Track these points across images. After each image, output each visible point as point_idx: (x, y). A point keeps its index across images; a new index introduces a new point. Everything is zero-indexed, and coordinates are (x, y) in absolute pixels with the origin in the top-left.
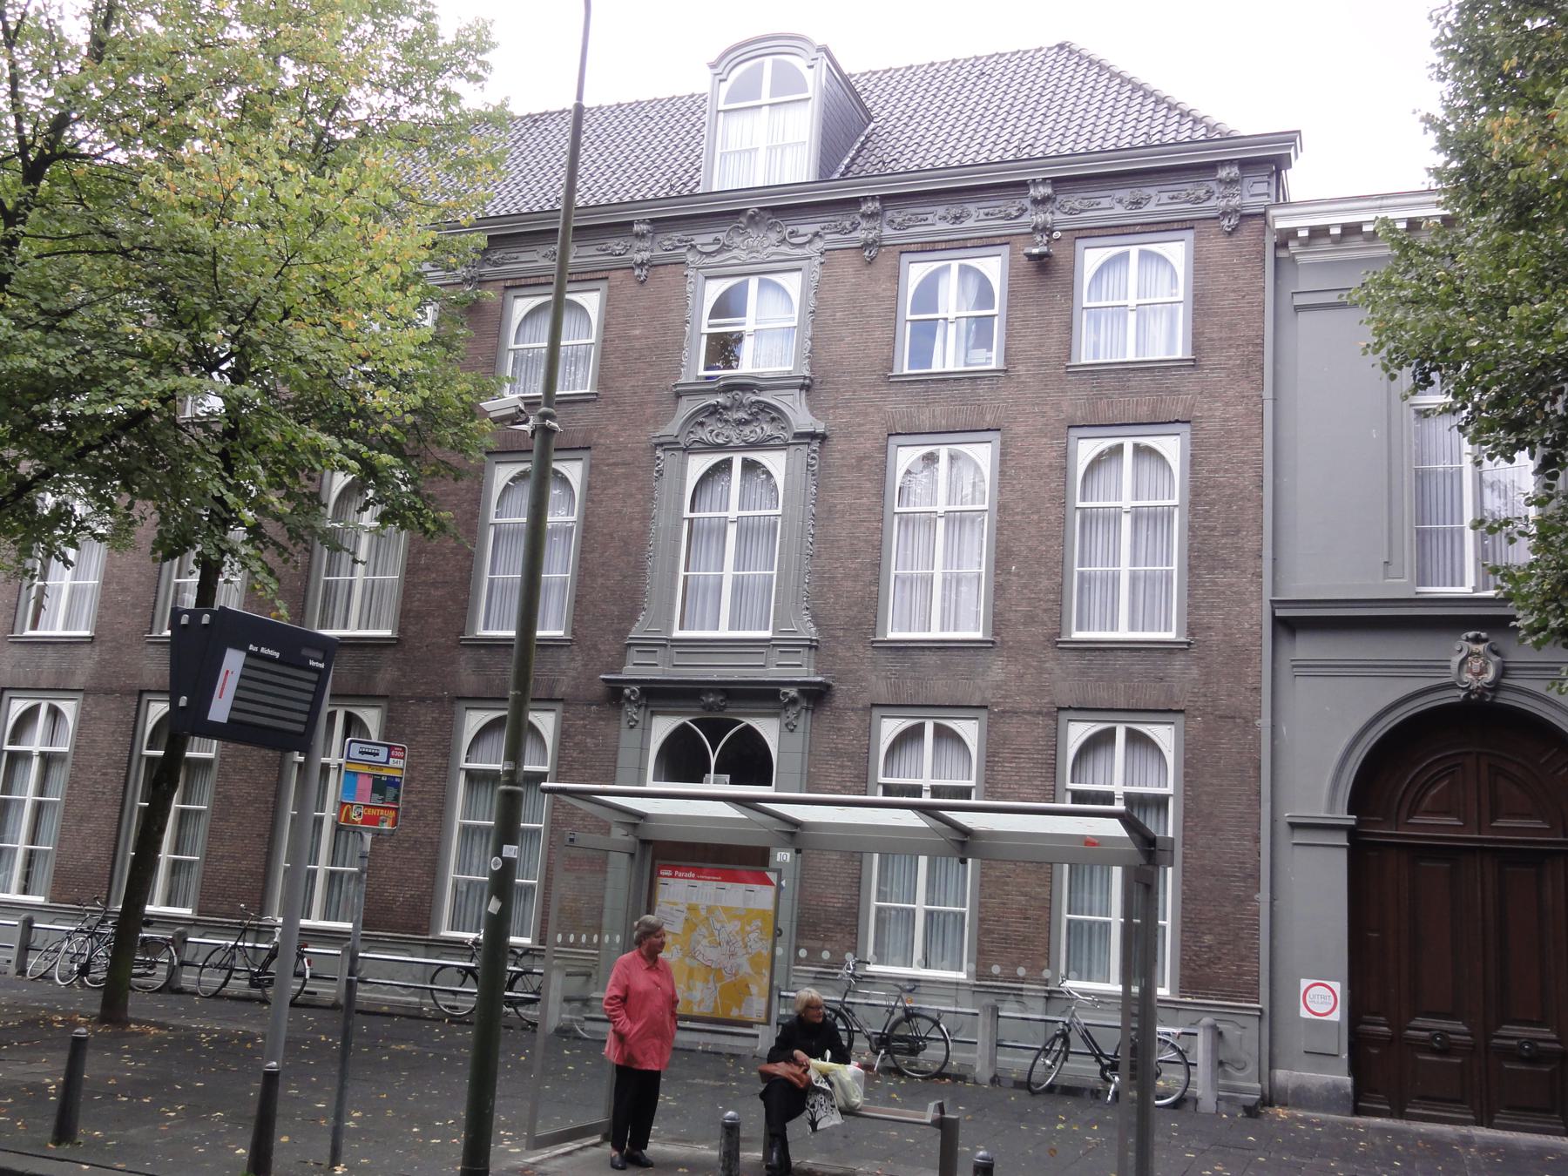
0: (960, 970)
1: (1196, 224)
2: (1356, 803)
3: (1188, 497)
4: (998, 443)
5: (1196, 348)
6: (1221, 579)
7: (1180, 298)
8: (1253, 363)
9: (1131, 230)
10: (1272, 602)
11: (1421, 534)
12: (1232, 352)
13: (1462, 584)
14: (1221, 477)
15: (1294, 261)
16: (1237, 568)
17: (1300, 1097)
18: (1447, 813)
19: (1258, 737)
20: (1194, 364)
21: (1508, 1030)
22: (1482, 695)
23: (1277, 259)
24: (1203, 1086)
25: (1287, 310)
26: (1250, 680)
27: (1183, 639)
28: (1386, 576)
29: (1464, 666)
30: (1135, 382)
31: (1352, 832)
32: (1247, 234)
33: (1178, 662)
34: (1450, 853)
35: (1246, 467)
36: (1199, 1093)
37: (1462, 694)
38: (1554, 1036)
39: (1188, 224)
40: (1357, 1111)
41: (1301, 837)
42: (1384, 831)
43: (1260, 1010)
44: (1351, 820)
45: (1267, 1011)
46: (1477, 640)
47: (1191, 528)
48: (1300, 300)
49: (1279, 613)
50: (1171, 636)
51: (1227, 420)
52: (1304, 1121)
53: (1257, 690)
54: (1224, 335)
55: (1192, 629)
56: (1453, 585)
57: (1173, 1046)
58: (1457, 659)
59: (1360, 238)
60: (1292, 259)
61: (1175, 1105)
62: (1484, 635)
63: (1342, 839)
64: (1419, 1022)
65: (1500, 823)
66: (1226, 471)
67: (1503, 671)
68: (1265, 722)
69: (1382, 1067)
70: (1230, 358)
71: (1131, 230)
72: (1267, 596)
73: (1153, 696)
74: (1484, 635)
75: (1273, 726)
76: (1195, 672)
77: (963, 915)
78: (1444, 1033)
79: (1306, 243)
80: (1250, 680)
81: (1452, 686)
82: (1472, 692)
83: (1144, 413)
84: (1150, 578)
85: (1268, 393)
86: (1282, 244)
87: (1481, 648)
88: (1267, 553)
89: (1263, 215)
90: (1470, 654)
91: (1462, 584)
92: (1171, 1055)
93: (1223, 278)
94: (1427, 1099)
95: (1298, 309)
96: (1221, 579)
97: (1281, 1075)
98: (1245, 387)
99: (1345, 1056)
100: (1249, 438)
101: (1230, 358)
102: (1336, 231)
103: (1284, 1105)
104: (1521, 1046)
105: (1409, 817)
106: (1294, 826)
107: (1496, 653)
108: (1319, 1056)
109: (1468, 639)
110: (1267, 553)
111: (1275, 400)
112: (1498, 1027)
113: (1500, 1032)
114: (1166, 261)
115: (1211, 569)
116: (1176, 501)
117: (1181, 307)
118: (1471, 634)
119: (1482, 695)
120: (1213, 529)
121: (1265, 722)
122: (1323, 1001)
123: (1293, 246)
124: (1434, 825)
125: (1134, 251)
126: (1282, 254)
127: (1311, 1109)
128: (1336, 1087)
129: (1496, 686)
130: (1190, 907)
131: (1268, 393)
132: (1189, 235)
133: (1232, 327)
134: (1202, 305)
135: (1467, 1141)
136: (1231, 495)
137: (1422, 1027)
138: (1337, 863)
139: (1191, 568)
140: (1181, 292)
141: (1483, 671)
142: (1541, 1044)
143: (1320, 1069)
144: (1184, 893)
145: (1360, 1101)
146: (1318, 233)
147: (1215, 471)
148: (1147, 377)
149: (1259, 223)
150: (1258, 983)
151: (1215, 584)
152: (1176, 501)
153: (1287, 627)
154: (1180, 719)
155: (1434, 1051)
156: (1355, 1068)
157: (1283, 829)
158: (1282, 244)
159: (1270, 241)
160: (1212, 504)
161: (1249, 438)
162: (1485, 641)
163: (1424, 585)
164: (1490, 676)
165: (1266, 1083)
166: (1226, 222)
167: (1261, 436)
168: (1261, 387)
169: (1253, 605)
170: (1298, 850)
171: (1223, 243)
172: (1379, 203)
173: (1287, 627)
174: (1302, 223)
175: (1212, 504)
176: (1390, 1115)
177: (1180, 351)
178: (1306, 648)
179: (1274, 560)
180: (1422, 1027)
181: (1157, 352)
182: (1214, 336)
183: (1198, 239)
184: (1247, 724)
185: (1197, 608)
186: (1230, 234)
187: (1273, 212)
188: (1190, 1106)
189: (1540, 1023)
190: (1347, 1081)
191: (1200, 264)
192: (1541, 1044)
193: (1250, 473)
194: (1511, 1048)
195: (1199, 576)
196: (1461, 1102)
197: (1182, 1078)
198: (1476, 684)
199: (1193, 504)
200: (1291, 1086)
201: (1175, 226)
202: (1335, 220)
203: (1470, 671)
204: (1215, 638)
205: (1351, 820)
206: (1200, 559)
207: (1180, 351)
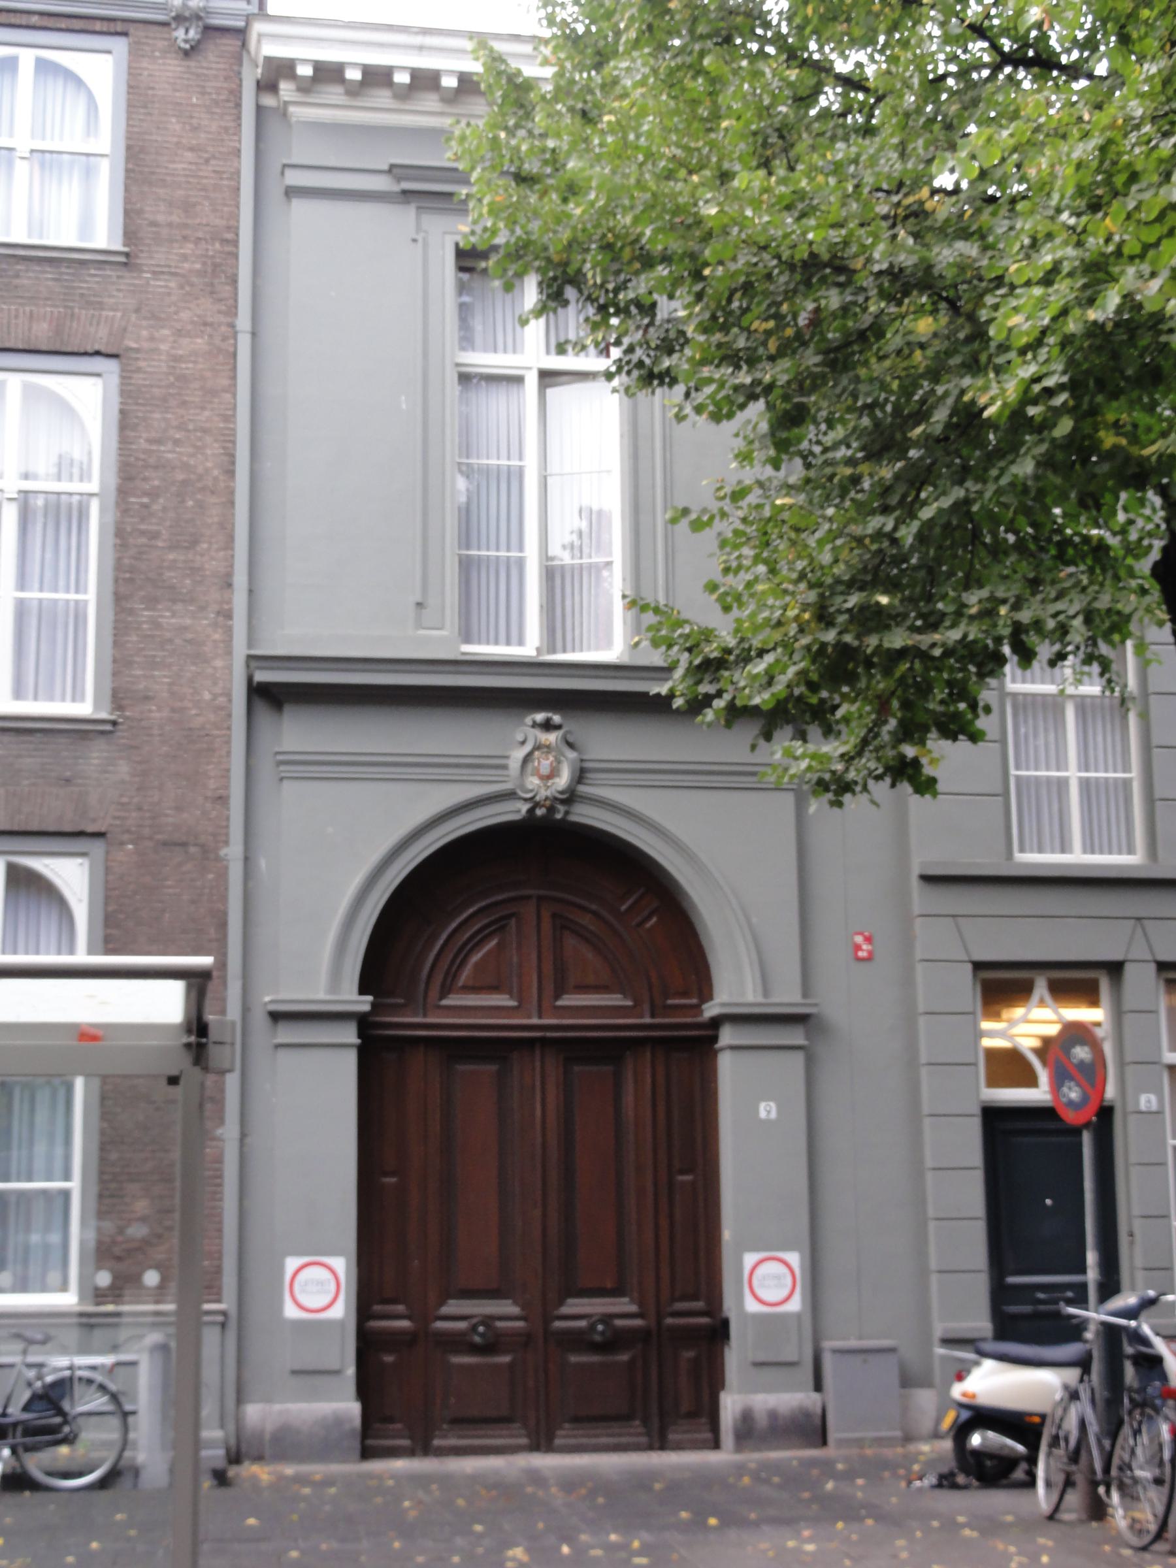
0: (64, 1288)
1: (132, 29)
2: (372, 977)
3: (113, 481)
4: (115, 380)
5: (129, 235)
6: (168, 619)
7: (106, 148)
8: (219, 273)
9: (24, 20)
10: (250, 658)
11: (467, 566)
12: (189, 248)
13: (521, 643)
14: (168, 453)
15: (285, 114)
16: (192, 601)
17: (284, 1444)
18: (495, 988)
19: (223, 875)
20: (127, 261)
21: (575, 1305)
22: (551, 810)
23: (259, 109)
24: (149, 1449)
25: (274, 192)
26: (212, 784)
27: (104, 715)
28: (419, 625)
29: (526, 767)
30: (28, 278)
31: (364, 1023)
32: (214, 57)
33: (97, 753)
34: (495, 1049)
35: (208, 439)
36: (141, 1457)
37: (524, 808)
38: (633, 1308)
39: (119, 27)
40: (367, 1453)
41: (288, 1033)
42: (409, 1020)
43: (224, 1313)
44: (364, 1004)
45: (233, 1313)
46: (547, 726)
47: (120, 533)
48: (294, 178)
49: (261, 677)
50: (84, 709)
51: (177, 359)
52: (300, 1480)
53: (222, 800)
54: (175, 219)
55: (118, 698)
56: (508, 643)
57: (102, 1388)
58: (519, 754)
59: (339, 89)
60: (282, 112)
61: (103, 1484)
62: (557, 719)
63: (349, 1034)
64: (453, 1307)
65: (567, 1001)
66: (177, 442)
67: (581, 775)
68: (233, 851)
69: (404, 1385)
70: (185, 258)
71: (24, 20)
72: (240, 651)
73: (54, 810)
74: (557, 719)
75: (246, 859)
76: (123, 769)
77: (66, 1195)
78: (488, 1320)
79: (307, 87)
80: (212, 784)
81: (510, 795)
82: (537, 805)
83: (41, 333)
84: (48, 614)
85: (243, 322)
86: (267, 86)
87: (552, 737)
88: (240, 579)
89: (241, 33)
90: (538, 747)
91: (521, 643)
92: (99, 1402)
93: (174, 125)
94: (461, 1422)
95: (291, 192)
96: (168, 619)
97: (253, 1412)
98: (206, 307)
99: (351, 1371)
100: (214, 393)
101: (185, 258)
102: (449, 82)
103: (259, 1458)
104: (592, 1327)
105: (442, 997)
106: (276, 1017)
107: (571, 745)
108: (310, 1375)
109: (535, 725)
110: (240, 579)
111: (254, 334)
112: (561, 1303)
113: (565, 1310)
114: (79, 82)
115: (152, 602)
116: (93, 486)
117: (104, 166)
118: (540, 717)
119: (551, 810)
120: (155, 536)
121: (233, 851)
122: (319, 1288)
123: (286, 89)
124: (474, 1006)
125: (27, 58)
126: (268, 101)
127: (301, 1460)
128: (339, 1420)
129: (570, 797)
130: (114, 1156)
131: (243, 322)
132: (120, 45)
133: (188, 207)
134: (140, 165)
135: (536, 1478)
136: (184, 483)
137: (460, 1313)
138: (344, 1069)
139: (118, 598)
140: (105, 139)
141: (554, 773)
142: (499, 1324)
143: (313, 1395)
144: (102, 1133)
145: (371, 1440)
146: (328, 73)
147: (158, 442)
148: (49, 273)
149: (230, 44)
150: (218, 1271)
151: (157, 625)
152: (93, 486)
153: (268, 696)
154: (97, 848)
155: (475, 1349)
156: (364, 1390)
157: (260, 1020)
158: (267, 86)
159: (250, 75)
160: (154, 494)
161: (214, 393)
162: (558, 727)
163: (468, 640)
164: (563, 781)
165: (231, 1427)
166: (180, 34)
167: (232, 389)
168: (233, 311)
169: (219, 663)
170: (282, 1054)
171: (174, 66)
172: (419, 40)
173: (268, 696)
174: (305, 54)
175: (154, 494)
176: (410, 1453)
177: (104, 235)
178: (298, 733)
179: (251, 591)
180: (460, 1313)
181: (63, 234)
182: (161, 218)
183: (135, 53)
184: (208, 855)
185: (129, 664)
186: (186, 54)
187: (258, 27)
188: (126, 1482)
189: (617, 1291)
190: (353, 1408)
191: (137, 96)
192: (499, 1324)
193: (214, 449)
194: (580, 1332)
195: (131, 612)
196: (624, 1418)
197: (115, 1436)
198: (543, 794)
199: (123, 492)
200: (269, 1427)
201: (98, 26)
202: (355, 57)
203: (536, 772)
204: (156, 714)
205: (364, 1004)
206: (136, 583)
207: (104, 235)
